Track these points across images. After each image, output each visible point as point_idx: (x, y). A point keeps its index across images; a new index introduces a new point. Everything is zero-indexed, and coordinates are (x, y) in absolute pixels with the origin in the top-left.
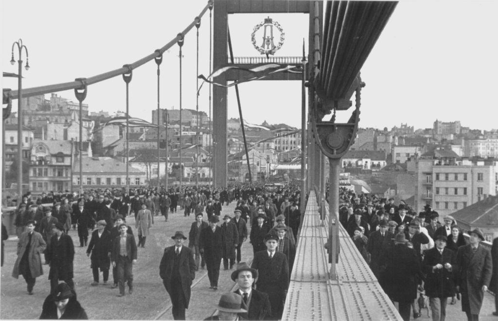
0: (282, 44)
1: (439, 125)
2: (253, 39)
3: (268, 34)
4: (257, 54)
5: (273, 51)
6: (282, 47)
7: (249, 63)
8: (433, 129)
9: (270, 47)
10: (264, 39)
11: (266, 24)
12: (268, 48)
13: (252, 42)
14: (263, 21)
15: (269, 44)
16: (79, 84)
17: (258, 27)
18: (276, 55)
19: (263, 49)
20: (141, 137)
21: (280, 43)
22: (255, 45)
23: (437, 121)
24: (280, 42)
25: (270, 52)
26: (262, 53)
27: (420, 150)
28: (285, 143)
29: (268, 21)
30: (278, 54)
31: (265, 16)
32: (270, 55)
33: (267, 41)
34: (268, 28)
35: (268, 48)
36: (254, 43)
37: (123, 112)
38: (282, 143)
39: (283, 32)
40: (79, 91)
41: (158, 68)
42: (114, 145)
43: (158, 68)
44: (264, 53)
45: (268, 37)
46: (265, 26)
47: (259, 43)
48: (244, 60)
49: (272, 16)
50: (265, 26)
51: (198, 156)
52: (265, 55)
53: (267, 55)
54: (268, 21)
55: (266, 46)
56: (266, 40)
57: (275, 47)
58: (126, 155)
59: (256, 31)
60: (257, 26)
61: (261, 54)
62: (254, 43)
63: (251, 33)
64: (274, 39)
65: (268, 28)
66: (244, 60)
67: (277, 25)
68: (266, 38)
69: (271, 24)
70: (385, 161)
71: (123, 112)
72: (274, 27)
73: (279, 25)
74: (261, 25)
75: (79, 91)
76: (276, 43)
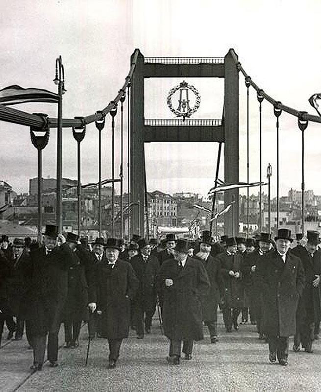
0: (198, 107)
1: (294, 193)
2: (168, 102)
3: (184, 97)
4: (173, 116)
5: (189, 114)
6: (198, 110)
7: (177, 125)
8: (289, 197)
9: (186, 109)
10: (180, 102)
11: (182, 88)
12: (184, 111)
13: (169, 105)
14: (179, 84)
15: (185, 107)
16: (79, 122)
17: (174, 91)
18: (191, 118)
19: (179, 112)
20: (23, 203)
21: (196, 106)
22: (171, 108)
23: (292, 190)
24: (196, 105)
25: (187, 115)
26: (179, 116)
27: (288, 215)
28: (160, 208)
29: (184, 85)
30: (194, 116)
31: (181, 80)
32: (186, 118)
33: (183, 103)
34: (184, 92)
35: (184, 111)
36: (170, 106)
37: (2, 181)
38: (157, 208)
39: (199, 95)
40: (77, 131)
41: (113, 120)
42: (2, 210)
43: (113, 120)
44: (180, 116)
45: (184, 100)
46: (181, 90)
47: (175, 106)
48: (169, 122)
49: (187, 80)
50: (181, 90)
51: (84, 220)
52: (182, 118)
53: (184, 117)
54: (184, 85)
55: (182, 109)
56: (182, 104)
57: (191, 110)
58: (190, 245)
59: (172, 94)
60: (173, 89)
61: (177, 117)
62: (170, 106)
63: (166, 97)
64: (189, 103)
65: (184, 92)
66: (171, 122)
67: (193, 89)
68: (182, 101)
69: (186, 88)
70: (256, 225)
71: (2, 181)
72: (190, 91)
73: (195, 89)
74: (177, 89)
75: (77, 131)
76: (192, 105)
